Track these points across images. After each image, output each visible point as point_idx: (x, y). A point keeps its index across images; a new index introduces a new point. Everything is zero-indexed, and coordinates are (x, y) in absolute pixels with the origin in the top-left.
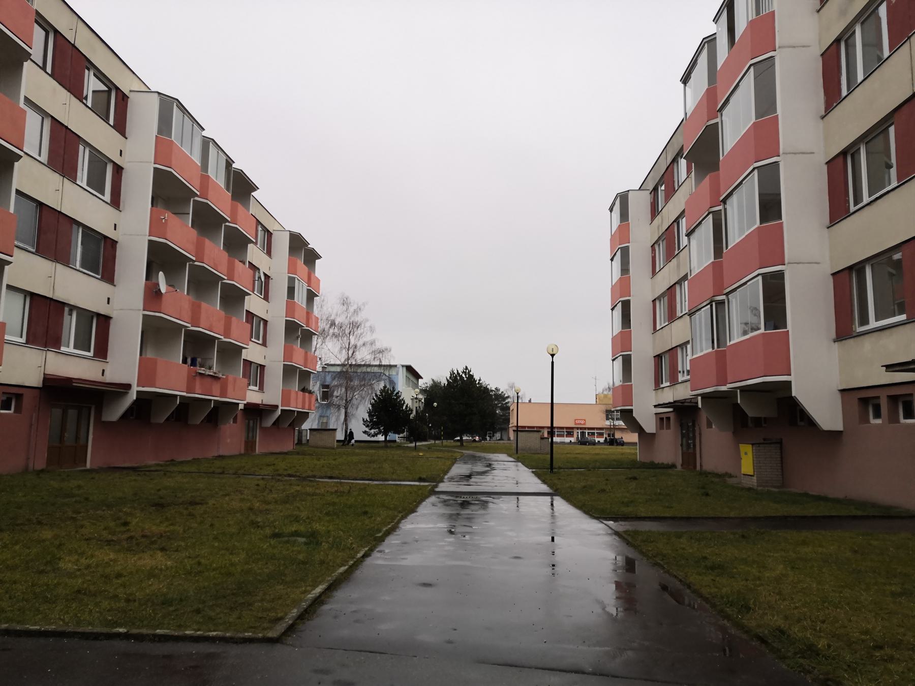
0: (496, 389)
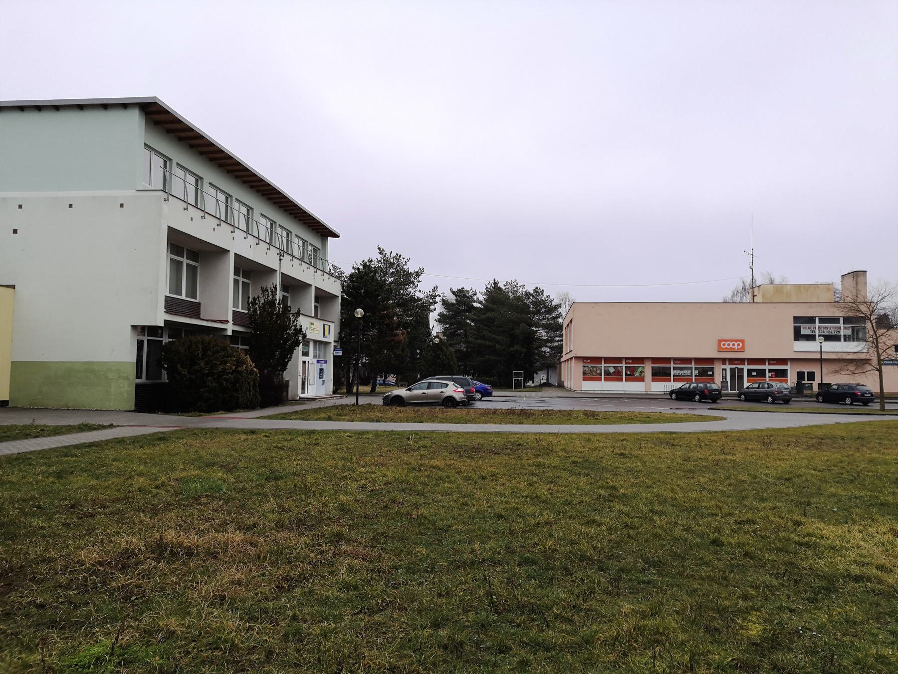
0: (536, 290)
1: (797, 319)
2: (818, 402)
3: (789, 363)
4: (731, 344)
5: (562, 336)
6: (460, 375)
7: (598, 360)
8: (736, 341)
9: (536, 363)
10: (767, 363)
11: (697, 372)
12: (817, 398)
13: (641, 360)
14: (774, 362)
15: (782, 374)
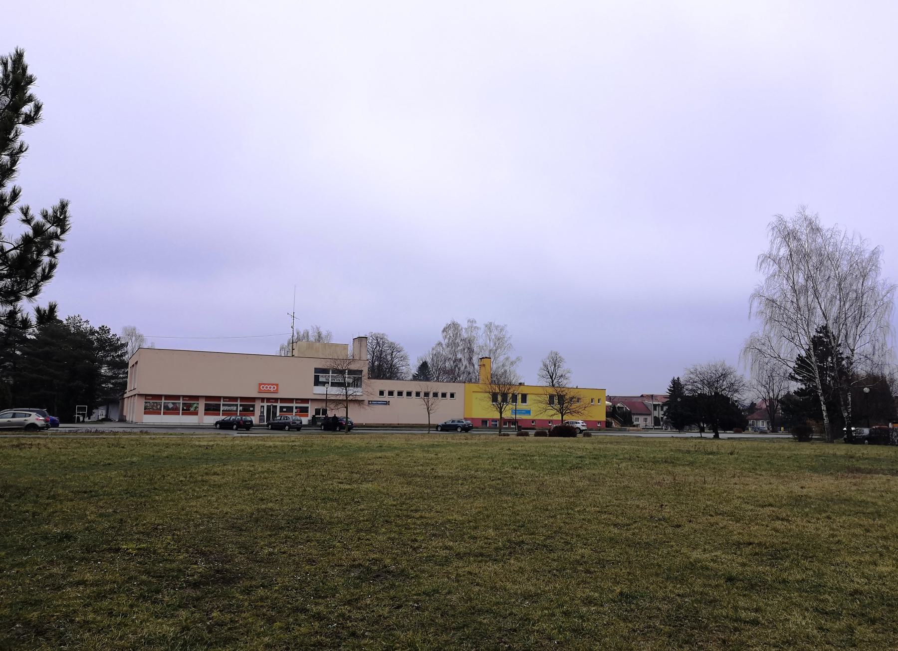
1: (317, 370)
2: (321, 429)
3: (310, 403)
4: (268, 387)
5: (127, 373)
6: (38, 408)
7: (159, 397)
8: (272, 385)
9: (98, 398)
10: (294, 402)
11: (241, 408)
12: (321, 427)
13: (196, 398)
14: (300, 401)
15: (304, 411)
